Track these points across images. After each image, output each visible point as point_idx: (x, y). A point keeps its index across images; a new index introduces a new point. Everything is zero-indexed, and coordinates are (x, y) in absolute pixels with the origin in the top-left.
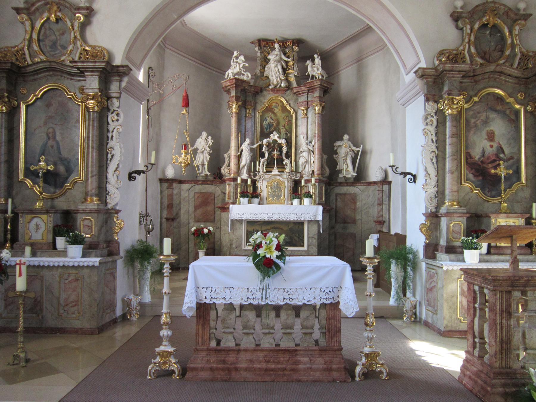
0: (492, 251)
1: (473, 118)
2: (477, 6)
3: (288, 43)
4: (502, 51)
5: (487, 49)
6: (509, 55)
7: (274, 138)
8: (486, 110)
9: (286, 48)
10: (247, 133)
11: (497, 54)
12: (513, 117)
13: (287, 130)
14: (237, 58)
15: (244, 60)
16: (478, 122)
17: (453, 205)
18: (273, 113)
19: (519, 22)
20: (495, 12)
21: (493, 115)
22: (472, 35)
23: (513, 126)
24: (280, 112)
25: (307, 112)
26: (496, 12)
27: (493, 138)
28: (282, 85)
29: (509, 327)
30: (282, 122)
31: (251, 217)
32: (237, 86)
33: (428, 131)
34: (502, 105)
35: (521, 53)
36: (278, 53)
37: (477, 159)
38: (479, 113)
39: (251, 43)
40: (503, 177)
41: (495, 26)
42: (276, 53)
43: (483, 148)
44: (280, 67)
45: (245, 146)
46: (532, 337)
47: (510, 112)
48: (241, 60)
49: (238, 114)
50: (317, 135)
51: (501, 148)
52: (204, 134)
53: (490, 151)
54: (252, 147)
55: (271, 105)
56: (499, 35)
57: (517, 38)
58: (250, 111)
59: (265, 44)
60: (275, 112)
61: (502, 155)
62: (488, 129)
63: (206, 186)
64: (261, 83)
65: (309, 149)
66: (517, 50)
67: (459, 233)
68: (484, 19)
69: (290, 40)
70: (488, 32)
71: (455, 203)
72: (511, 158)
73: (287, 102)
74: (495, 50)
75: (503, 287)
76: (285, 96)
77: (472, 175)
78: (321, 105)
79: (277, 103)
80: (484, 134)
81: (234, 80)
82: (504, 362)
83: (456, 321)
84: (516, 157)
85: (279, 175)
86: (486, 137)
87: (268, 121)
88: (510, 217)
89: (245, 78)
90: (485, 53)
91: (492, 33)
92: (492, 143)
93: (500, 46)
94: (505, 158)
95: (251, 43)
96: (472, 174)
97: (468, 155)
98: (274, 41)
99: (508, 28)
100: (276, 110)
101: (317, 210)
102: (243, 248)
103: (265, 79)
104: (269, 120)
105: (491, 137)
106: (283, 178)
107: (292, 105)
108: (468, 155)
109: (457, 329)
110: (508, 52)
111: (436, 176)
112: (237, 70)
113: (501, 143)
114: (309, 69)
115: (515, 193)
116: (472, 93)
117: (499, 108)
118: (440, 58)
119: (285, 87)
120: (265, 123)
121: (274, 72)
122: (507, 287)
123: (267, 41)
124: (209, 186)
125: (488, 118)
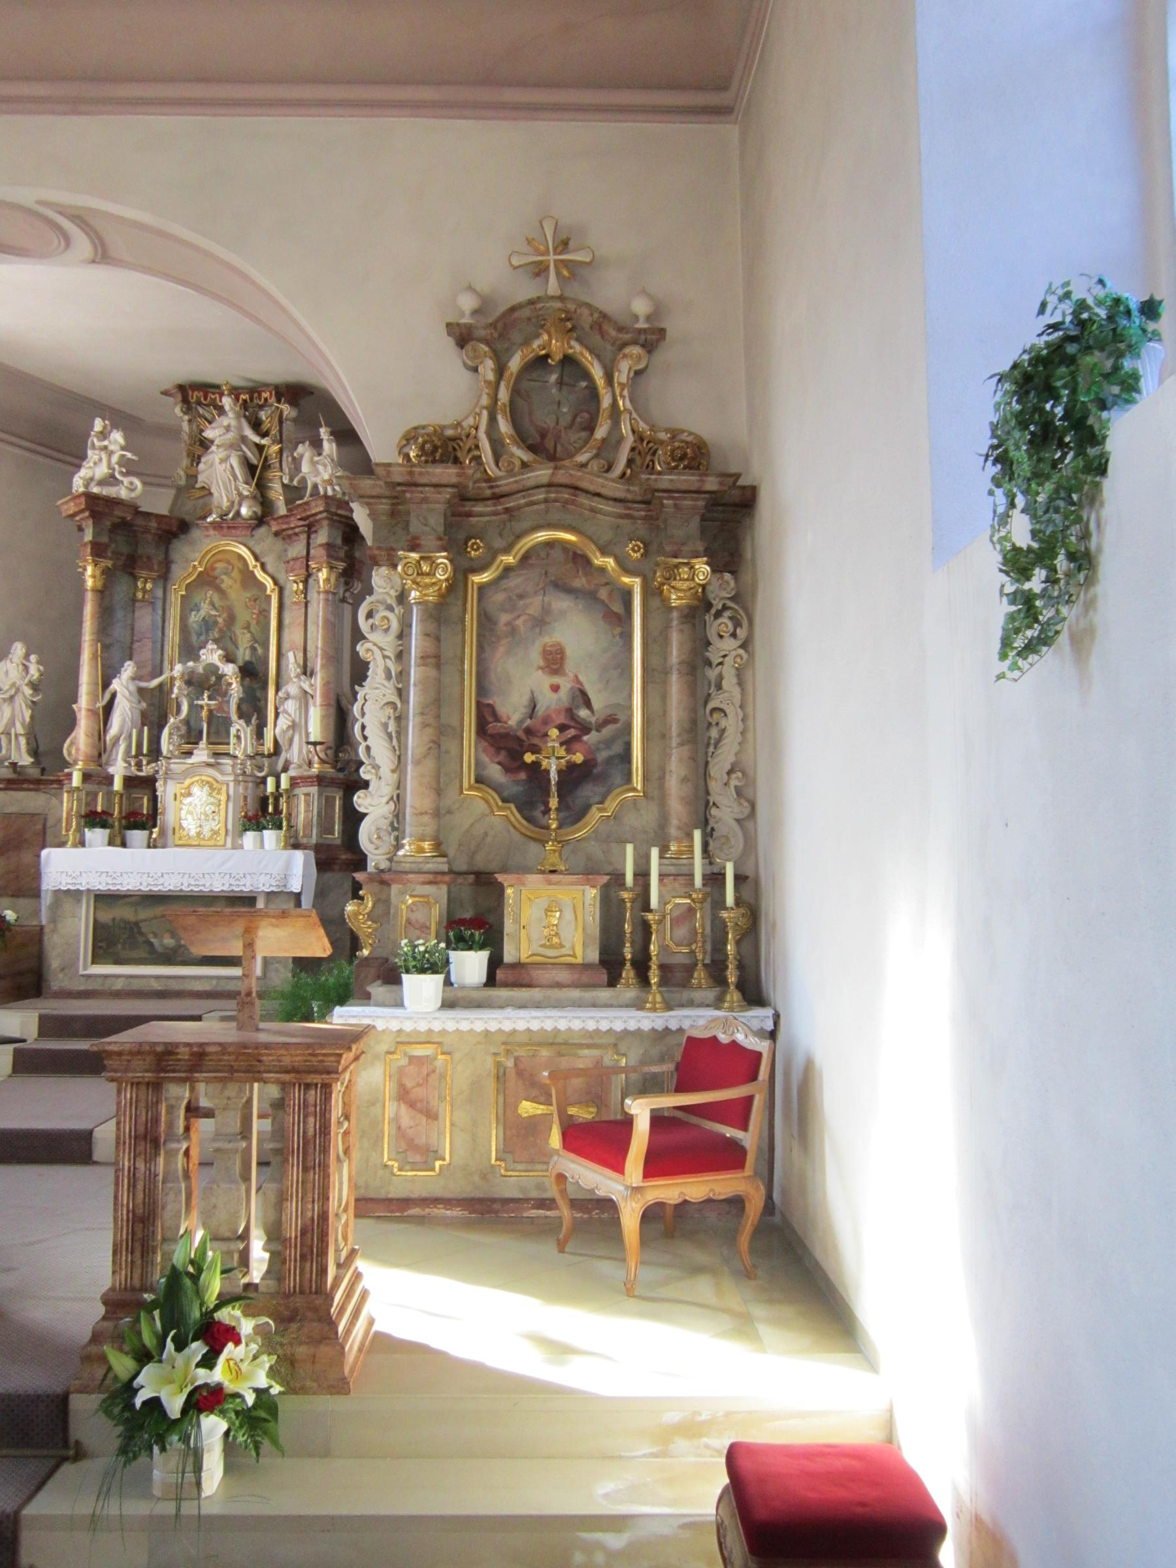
0: (500, 975)
1: (506, 611)
2: (513, 309)
3: (265, 395)
4: (590, 428)
5: (550, 422)
6: (604, 440)
7: (210, 661)
8: (543, 588)
9: (261, 407)
10: (136, 645)
11: (576, 436)
12: (617, 608)
13: (254, 640)
14: (103, 435)
15: (122, 441)
16: (519, 622)
17: (421, 850)
18: (219, 589)
19: (627, 350)
20: (569, 325)
21: (561, 603)
22: (503, 385)
23: (618, 630)
24: (237, 586)
25: (306, 588)
26: (569, 325)
27: (562, 665)
28: (244, 511)
29: (152, 1177)
30: (244, 615)
31: (102, 884)
32: (96, 516)
33: (375, 649)
34: (586, 575)
35: (633, 432)
36: (233, 423)
37: (512, 722)
38: (521, 597)
39: (162, 393)
40: (554, 776)
41: (568, 361)
42: (225, 423)
43: (532, 693)
44: (235, 461)
45: (122, 685)
46: (215, 1207)
47: (610, 594)
48: (116, 441)
49: (102, 593)
50: (319, 652)
51: (583, 693)
52: (19, 649)
53: (549, 702)
54: (144, 684)
55: (213, 569)
56: (584, 384)
57: (626, 393)
58: (149, 586)
59: (196, 396)
60: (223, 586)
61: (583, 713)
62: (547, 640)
63: (21, 795)
64: (187, 510)
65: (306, 692)
66: (625, 429)
67: (424, 928)
68: (536, 344)
69: (266, 385)
70: (553, 378)
71: (426, 845)
72: (610, 720)
73: (257, 558)
74: (570, 426)
75: (135, 1071)
76: (251, 543)
77: (498, 767)
78: (331, 568)
79: (228, 562)
80: (535, 656)
81: (83, 500)
82: (137, 1276)
83: (380, 1172)
84: (622, 718)
85: (209, 765)
86: (542, 663)
87: (202, 613)
88: (556, 883)
89: (123, 494)
90: (543, 435)
91: (566, 379)
92: (556, 680)
93: (586, 415)
94: (593, 720)
95: (162, 393)
96: (499, 763)
97: (486, 716)
98: (217, 387)
99: (605, 367)
100: (226, 582)
101: (288, 865)
102: (82, 972)
103: (199, 494)
104: (205, 610)
105: (554, 661)
106: (223, 774)
107: (269, 567)
108: (486, 716)
109: (382, 1195)
110: (601, 433)
111: (393, 771)
112: (102, 471)
113: (581, 678)
114: (305, 468)
115: (616, 817)
116: (498, 543)
117: (580, 582)
118: (405, 450)
119: (251, 518)
120: (194, 618)
121: (222, 474)
122: (147, 1071)
123: (207, 388)
124: (32, 794)
125: (546, 610)
